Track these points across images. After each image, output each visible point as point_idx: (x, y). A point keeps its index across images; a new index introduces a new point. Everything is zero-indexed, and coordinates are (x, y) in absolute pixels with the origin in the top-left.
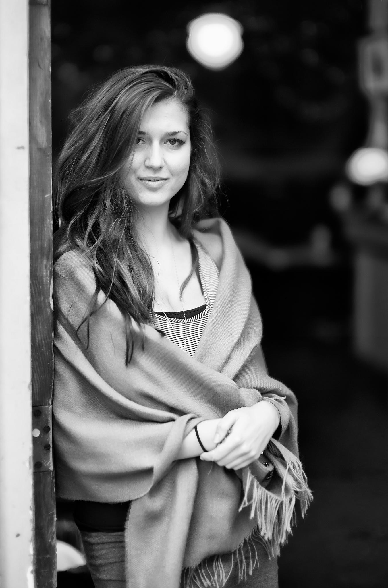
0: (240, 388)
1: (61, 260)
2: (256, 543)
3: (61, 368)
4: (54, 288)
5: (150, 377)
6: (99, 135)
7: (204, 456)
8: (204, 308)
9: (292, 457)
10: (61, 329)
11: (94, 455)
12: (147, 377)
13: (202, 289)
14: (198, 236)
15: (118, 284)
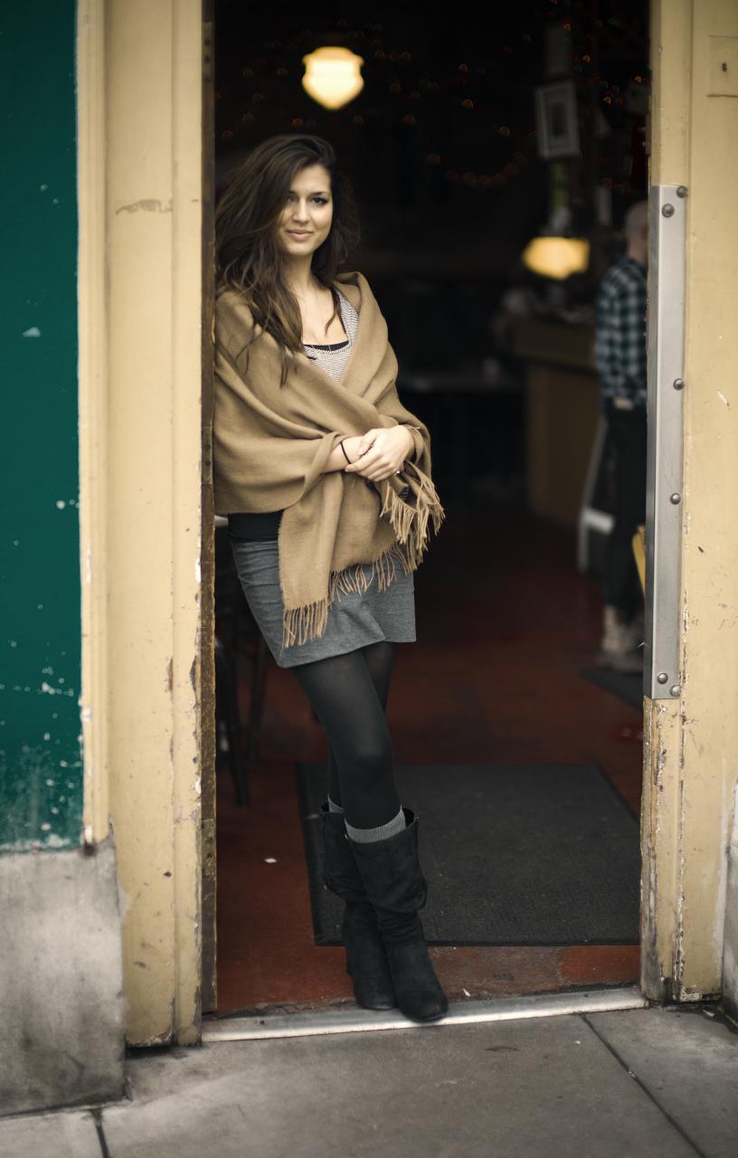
0: (380, 413)
1: (220, 299)
2: (394, 558)
3: (222, 393)
4: (216, 324)
5: (301, 398)
6: (253, 194)
7: (349, 468)
8: (346, 343)
9: (426, 479)
10: (221, 358)
11: (252, 468)
12: (299, 398)
13: (342, 336)
14: (340, 286)
15: (273, 320)
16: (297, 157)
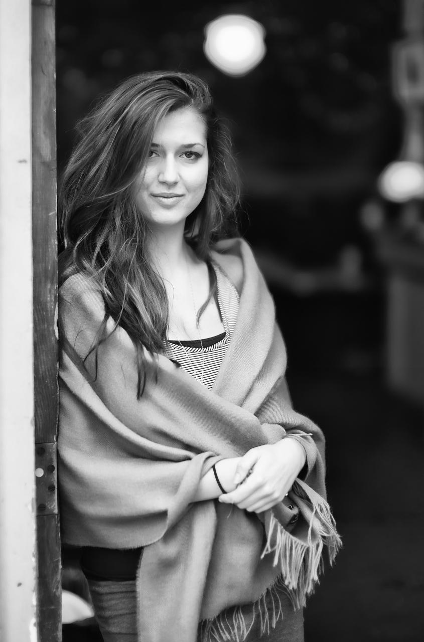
0: (262, 423)
1: (67, 284)
2: (280, 593)
4: (59, 315)
5: (163, 411)
6: (109, 147)
7: (223, 498)
8: (223, 336)
9: (319, 500)
10: (67, 359)
11: (102, 497)
12: (160, 412)
13: (221, 316)
14: (217, 257)
15: (129, 310)
16: (162, 99)
